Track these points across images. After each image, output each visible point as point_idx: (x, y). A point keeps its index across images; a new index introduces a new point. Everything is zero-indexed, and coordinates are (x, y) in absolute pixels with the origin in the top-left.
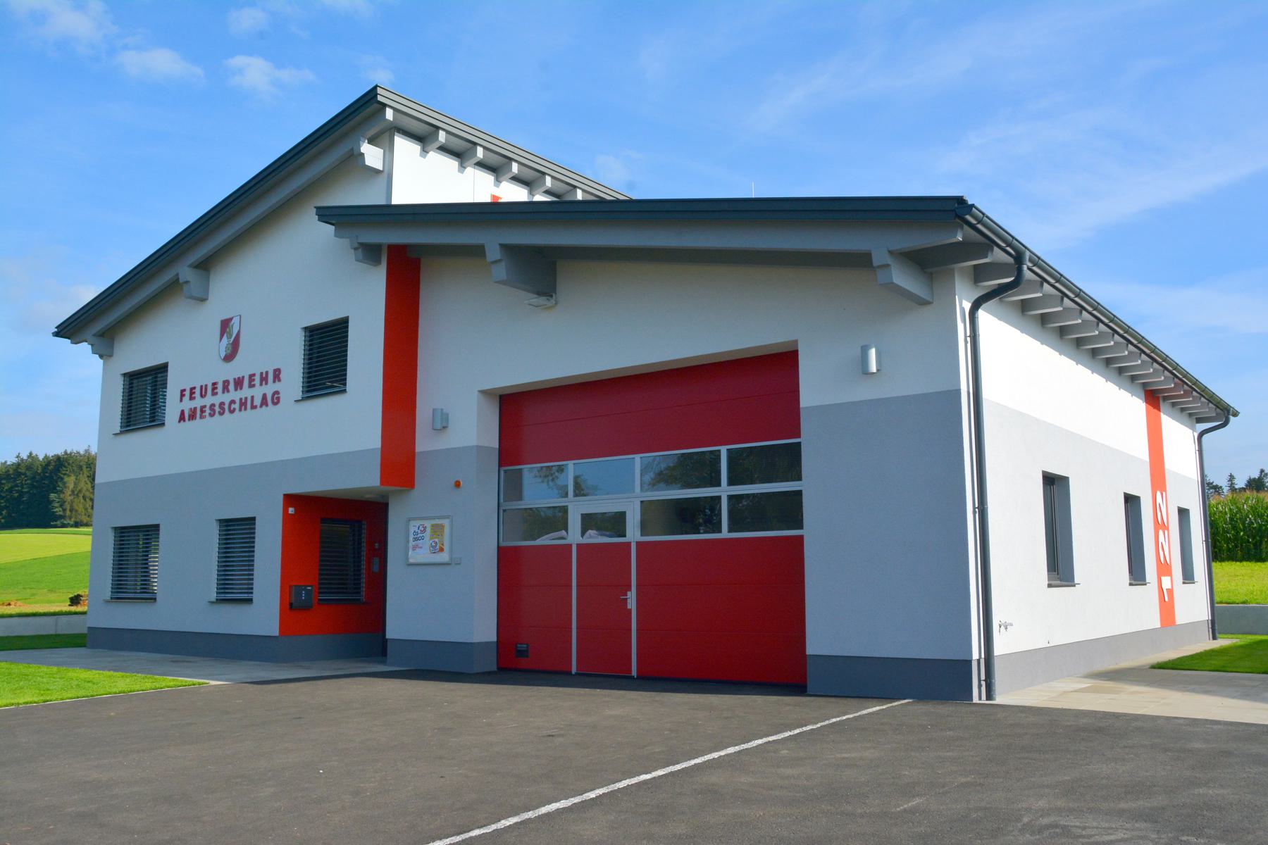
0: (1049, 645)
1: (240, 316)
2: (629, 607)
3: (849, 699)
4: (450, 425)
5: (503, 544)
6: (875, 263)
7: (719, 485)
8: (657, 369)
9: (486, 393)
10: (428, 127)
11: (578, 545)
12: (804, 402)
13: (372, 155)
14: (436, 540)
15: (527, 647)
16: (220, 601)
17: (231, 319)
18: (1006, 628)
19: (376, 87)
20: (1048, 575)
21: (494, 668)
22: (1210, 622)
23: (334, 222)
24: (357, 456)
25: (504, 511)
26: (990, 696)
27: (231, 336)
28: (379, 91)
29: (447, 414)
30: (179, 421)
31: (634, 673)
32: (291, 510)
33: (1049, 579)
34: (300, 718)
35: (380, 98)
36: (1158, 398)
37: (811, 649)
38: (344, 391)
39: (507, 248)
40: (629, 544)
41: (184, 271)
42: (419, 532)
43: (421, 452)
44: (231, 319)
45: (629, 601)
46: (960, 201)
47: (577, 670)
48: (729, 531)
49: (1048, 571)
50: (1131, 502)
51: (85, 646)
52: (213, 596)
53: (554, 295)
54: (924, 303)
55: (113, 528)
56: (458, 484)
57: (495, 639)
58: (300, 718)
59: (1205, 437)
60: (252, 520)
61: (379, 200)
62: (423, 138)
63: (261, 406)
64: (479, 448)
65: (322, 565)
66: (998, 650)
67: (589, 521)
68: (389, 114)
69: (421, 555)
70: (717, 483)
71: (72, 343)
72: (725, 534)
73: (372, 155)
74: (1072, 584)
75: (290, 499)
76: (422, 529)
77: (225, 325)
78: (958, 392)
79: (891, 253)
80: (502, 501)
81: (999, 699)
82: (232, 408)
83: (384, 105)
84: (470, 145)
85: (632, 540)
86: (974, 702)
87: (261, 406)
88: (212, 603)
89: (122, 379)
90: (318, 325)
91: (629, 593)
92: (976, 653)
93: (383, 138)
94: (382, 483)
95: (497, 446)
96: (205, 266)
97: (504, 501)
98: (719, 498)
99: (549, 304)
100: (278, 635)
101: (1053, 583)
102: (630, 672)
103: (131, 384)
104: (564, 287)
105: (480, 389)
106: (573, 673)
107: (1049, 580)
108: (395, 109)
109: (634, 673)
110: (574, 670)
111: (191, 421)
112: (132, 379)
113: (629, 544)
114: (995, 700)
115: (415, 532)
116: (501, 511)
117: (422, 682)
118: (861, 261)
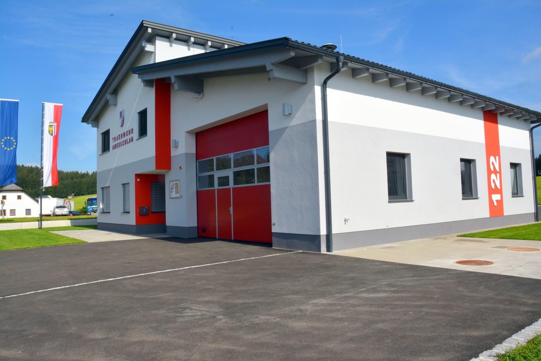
0: (387, 228)
2: (231, 213)
4: (179, 146)
5: (199, 190)
6: (268, 70)
9: (189, 132)
10: (170, 33)
11: (233, 188)
12: (270, 129)
13: (149, 48)
17: (122, 111)
18: (347, 221)
19: (143, 21)
20: (389, 197)
21: (197, 236)
22: (536, 213)
23: (138, 73)
24: (145, 161)
25: (198, 177)
26: (329, 248)
28: (144, 22)
29: (178, 142)
31: (233, 239)
32: (138, 180)
33: (389, 199)
34: (495, 241)
35: (144, 25)
36: (496, 114)
38: (147, 135)
39: (176, 77)
40: (215, 190)
41: (108, 96)
43: (173, 156)
44: (122, 111)
45: (231, 211)
46: (286, 39)
48: (257, 183)
49: (389, 195)
50: (468, 163)
53: (202, 93)
54: (304, 84)
57: (196, 225)
58: (495, 241)
59: (534, 130)
61: (152, 62)
62: (167, 36)
64: (186, 154)
65: (110, 202)
66: (334, 231)
68: (150, 30)
69: (174, 195)
70: (253, 164)
71: (87, 124)
73: (149, 48)
74: (522, 196)
75: (137, 176)
77: (121, 113)
78: (314, 121)
79: (273, 64)
80: (197, 173)
81: (334, 252)
83: (148, 27)
84: (189, 37)
86: (322, 253)
89: (101, 135)
91: (231, 207)
92: (323, 231)
93: (151, 40)
94: (157, 169)
95: (194, 152)
96: (115, 92)
97: (199, 173)
98: (254, 169)
99: (200, 97)
101: (464, 198)
102: (231, 238)
103: (104, 136)
104: (207, 90)
107: (389, 199)
108: (152, 28)
110: (217, 238)
112: (105, 135)
114: (332, 252)
116: (197, 177)
118: (261, 70)
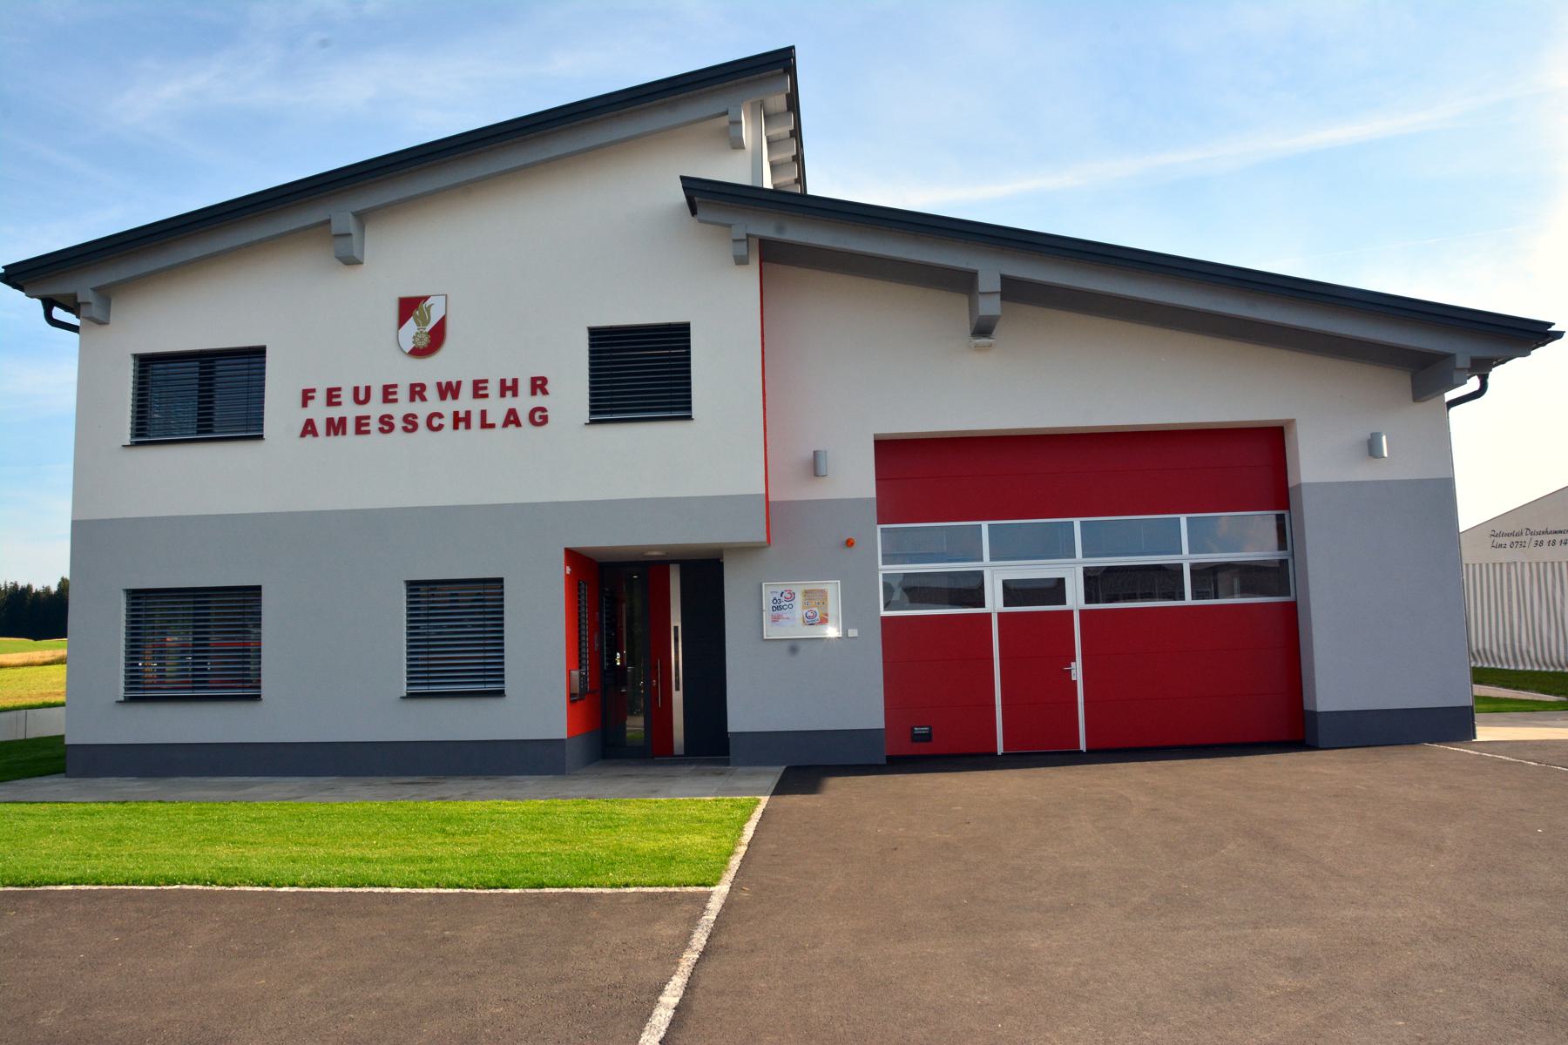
1: (446, 295)
2: (1073, 679)
3: (1335, 751)
7: (981, 559)
8: (1182, 428)
14: (816, 609)
15: (930, 730)
16: (130, 700)
27: (427, 323)
30: (303, 435)
31: (1083, 747)
37: (729, 731)
42: (783, 599)
45: (1073, 672)
47: (1004, 750)
51: (64, 772)
52: (121, 695)
55: (124, 590)
56: (849, 543)
60: (259, 588)
63: (505, 425)
67: (1013, 592)
72: (1188, 600)
76: (789, 596)
82: (541, 420)
85: (1075, 608)
87: (505, 425)
88: (120, 702)
90: (611, 328)
91: (1073, 664)
100: (566, 737)
102: (1078, 745)
105: (299, 434)
106: (999, 753)
109: (1083, 747)
111: (332, 437)
113: (989, 615)
115: (775, 599)
117: (1205, 761)
